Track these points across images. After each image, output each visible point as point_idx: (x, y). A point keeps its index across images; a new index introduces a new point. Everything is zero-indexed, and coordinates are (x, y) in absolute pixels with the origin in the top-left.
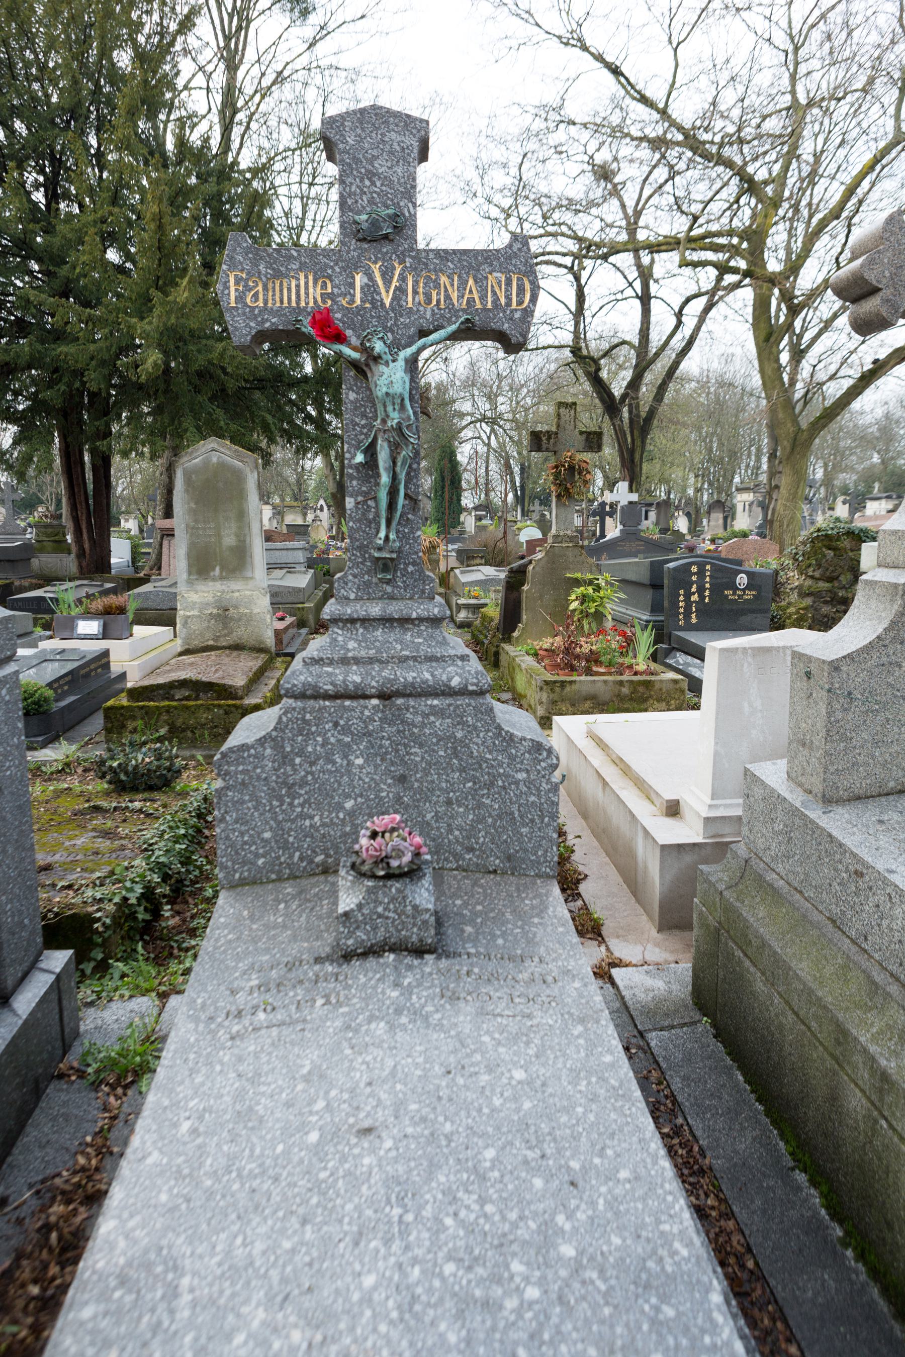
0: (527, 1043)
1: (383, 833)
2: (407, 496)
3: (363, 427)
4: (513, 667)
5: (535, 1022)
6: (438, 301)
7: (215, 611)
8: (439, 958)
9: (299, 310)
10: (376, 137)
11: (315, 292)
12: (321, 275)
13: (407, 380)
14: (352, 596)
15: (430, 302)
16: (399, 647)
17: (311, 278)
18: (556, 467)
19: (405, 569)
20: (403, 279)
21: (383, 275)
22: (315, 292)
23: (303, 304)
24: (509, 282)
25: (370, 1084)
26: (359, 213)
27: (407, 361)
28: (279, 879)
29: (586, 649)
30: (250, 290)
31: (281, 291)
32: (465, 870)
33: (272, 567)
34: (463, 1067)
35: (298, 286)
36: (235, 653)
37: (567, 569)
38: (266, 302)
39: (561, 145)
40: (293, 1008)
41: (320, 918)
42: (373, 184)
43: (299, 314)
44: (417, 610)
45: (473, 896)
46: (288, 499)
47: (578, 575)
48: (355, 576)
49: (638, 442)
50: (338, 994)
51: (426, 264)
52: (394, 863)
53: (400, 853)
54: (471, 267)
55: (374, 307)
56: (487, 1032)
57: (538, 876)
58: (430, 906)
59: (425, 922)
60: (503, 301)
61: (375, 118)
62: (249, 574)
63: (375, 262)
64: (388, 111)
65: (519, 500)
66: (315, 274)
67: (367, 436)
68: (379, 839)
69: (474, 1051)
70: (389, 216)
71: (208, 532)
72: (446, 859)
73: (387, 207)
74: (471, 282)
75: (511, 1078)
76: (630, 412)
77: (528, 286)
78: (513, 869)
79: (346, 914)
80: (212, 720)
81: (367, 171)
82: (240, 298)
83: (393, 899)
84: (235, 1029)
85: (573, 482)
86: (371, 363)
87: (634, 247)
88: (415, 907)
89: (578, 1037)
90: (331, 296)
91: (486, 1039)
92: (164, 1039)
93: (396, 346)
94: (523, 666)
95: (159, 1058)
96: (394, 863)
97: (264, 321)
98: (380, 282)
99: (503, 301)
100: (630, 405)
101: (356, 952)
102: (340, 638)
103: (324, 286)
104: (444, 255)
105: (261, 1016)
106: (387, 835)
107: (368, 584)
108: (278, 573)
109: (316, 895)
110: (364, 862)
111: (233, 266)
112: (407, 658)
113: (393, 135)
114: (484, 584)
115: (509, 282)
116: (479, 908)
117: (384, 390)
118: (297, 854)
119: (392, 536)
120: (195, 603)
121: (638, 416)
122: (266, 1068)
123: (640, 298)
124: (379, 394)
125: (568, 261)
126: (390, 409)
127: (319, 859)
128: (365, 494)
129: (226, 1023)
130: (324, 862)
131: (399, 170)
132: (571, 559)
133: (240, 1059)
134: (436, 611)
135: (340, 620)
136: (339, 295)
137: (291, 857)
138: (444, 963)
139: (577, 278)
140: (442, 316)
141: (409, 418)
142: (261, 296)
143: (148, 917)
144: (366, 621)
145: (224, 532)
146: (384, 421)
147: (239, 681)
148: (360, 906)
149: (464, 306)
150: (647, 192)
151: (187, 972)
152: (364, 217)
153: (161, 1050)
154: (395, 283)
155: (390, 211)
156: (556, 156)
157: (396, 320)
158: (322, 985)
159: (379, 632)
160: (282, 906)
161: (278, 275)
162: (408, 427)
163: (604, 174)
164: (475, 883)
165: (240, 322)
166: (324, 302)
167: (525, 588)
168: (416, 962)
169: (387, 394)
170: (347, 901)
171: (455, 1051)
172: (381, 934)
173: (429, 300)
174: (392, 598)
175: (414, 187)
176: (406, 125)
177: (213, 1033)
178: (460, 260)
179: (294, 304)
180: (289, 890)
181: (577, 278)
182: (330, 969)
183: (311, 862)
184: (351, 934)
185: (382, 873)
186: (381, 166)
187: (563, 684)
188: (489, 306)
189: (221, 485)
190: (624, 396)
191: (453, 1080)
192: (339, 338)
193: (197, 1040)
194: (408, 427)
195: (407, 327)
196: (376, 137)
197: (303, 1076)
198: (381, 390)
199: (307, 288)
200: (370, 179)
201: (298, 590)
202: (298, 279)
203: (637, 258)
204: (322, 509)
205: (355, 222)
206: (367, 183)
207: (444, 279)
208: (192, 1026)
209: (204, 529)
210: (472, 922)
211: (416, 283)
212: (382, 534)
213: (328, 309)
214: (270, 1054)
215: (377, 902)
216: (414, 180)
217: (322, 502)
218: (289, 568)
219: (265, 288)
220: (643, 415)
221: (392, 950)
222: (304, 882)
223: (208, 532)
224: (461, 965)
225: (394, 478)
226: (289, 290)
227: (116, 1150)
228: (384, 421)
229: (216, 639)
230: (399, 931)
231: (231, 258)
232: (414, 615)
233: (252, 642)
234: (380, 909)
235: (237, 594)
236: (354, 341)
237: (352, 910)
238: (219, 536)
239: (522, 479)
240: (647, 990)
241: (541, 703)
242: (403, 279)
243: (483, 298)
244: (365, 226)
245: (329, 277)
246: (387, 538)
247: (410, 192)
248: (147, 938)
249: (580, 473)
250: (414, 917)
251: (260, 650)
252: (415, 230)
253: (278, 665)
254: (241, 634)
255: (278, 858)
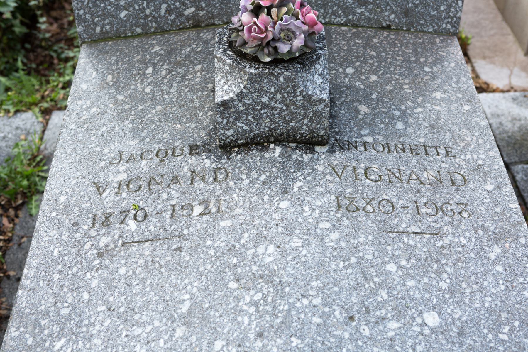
0: (439, 273)
1: (269, 8)
5: (446, 241)
8: (331, 151)
25: (260, 335)
28: (146, 34)
32: (355, 26)
34: (368, 311)
40: (167, 215)
41: (193, 89)
45: (365, 61)
50: (218, 201)
52: (284, 48)
53: (289, 35)
56: (394, 259)
57: (437, 33)
58: (325, 96)
59: (318, 114)
68: (263, 16)
69: (379, 287)
72: (334, 13)
75: (424, 324)
78: (410, 25)
79: (224, 104)
83: (280, 89)
84: (104, 241)
88: (307, 98)
89: (495, 262)
91: (391, 267)
92: (48, 159)
95: (45, 178)
96: (284, 48)
101: (237, 140)
105: (132, 225)
106: (274, 10)
109: (188, 56)
110: (245, 43)
116: (374, 78)
118: (164, 6)
122: (139, 301)
127: (189, 12)
129: (93, 233)
130: (195, 16)
133: (110, 286)
137: (157, 9)
138: (338, 158)
143: (24, 30)
148: (241, 96)
151: (67, 85)
153: (47, 171)
158: (199, 184)
160: (150, 70)
164: (367, 44)
168: (306, 158)
170: (226, 89)
171: (357, 287)
172: (265, 125)
177: (79, 245)
180: (157, 48)
182: (208, 162)
183: (181, 15)
184: (230, 125)
185: (268, 59)
191: (357, 329)
193: (62, 255)
197: (182, 317)
208: (54, 233)
210: (366, 98)
214: (143, 280)
215: (262, 92)
221: (279, 141)
222: (174, 38)
224: (358, 159)
227: (12, 273)
230: (287, 122)
234: (265, 99)
237: (232, 100)
240: (514, 120)
248: (28, 46)
250: (305, 108)
255: (143, 10)
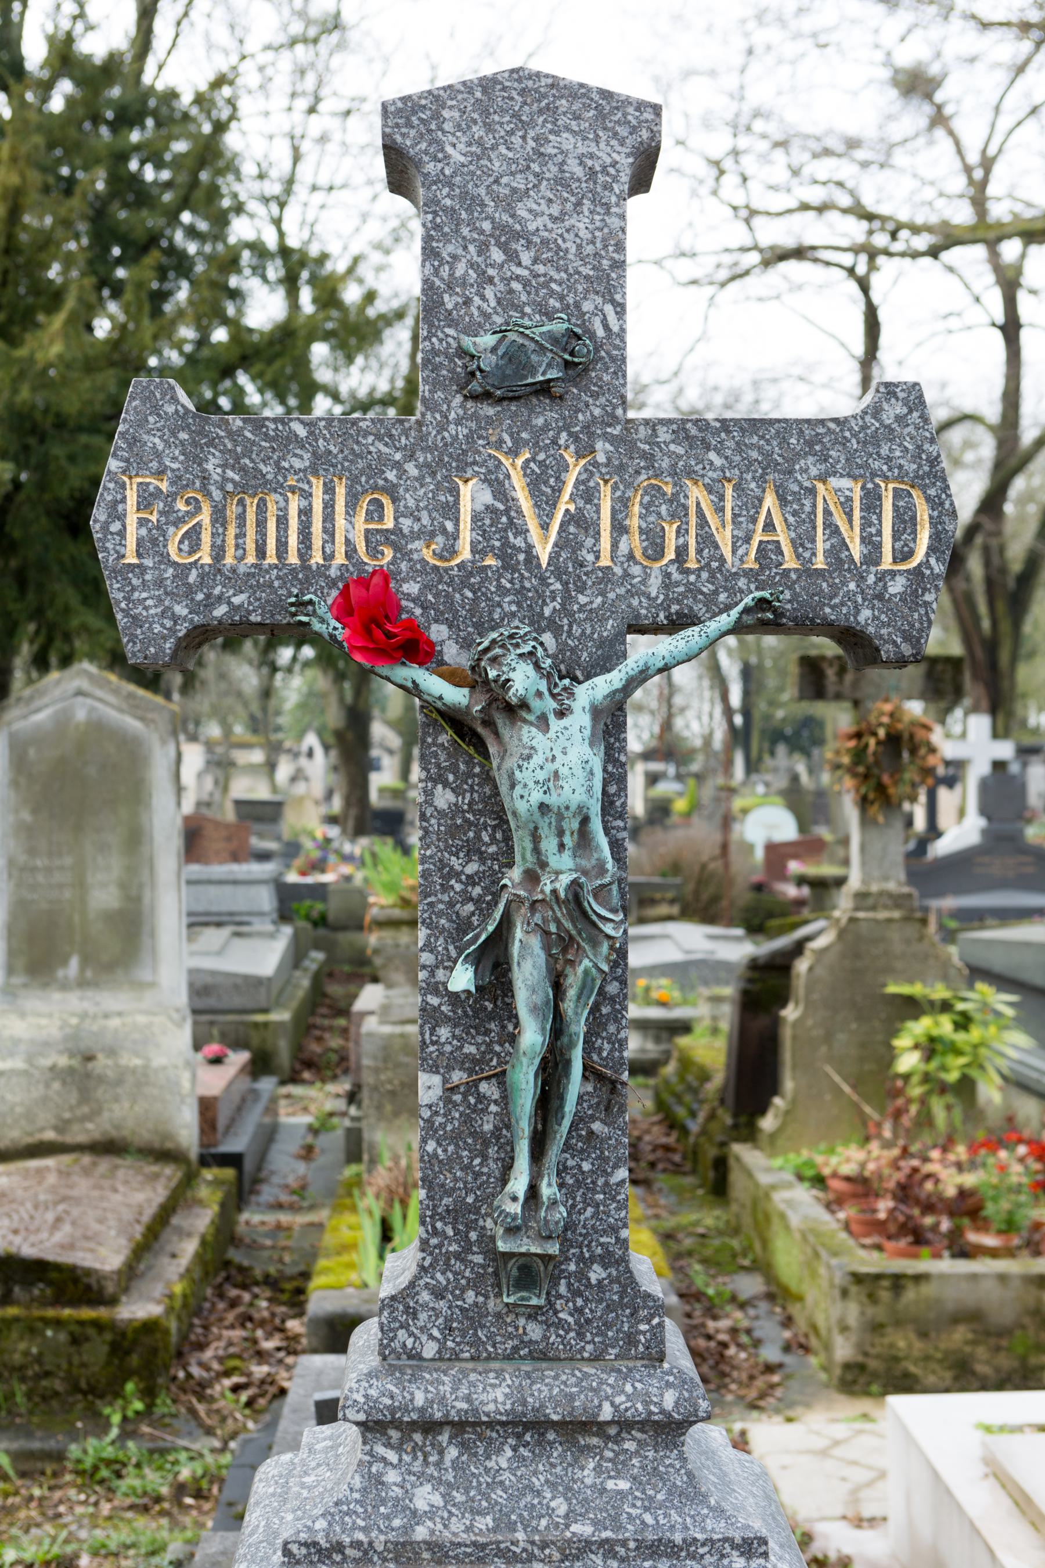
2: (588, 1069)
3: (471, 880)
4: (762, 1217)
6: (681, 552)
7: (63, 1061)
9: (306, 574)
10: (522, 145)
11: (353, 527)
12: (368, 484)
13: (597, 764)
14: (430, 1350)
15: (660, 554)
16: (560, 1506)
17: (341, 491)
18: (858, 735)
19: (582, 1275)
20: (587, 494)
21: (534, 485)
22: (353, 527)
23: (317, 558)
24: (872, 502)
26: (473, 330)
27: (596, 712)
29: (951, 1182)
30: (178, 522)
31: (261, 524)
33: (199, 921)
35: (306, 513)
36: (105, 1164)
37: (889, 971)
38: (219, 552)
39: (828, 30)
42: (513, 257)
43: (305, 584)
44: (615, 1394)
46: (238, 729)
47: (916, 989)
48: (438, 1294)
49: (1005, 627)
51: (649, 457)
54: (768, 464)
55: (508, 564)
60: (857, 550)
61: (520, 101)
62: (144, 974)
63: (514, 452)
64: (555, 83)
65: (739, 737)
66: (354, 480)
67: (484, 910)
70: (554, 339)
71: (58, 877)
73: (549, 315)
74: (770, 501)
76: (987, 563)
77: (923, 512)
80: (39, 1359)
81: (500, 228)
82: (152, 543)
85: (897, 769)
86: (500, 720)
87: (986, 233)
90: (395, 538)
93: (566, 672)
94: (795, 1220)
97: (211, 602)
98: (525, 503)
99: (857, 550)
100: (986, 551)
102: (392, 1476)
103: (376, 511)
104: (695, 432)
107: (474, 1317)
108: (213, 937)
111: (136, 463)
112: (586, 1546)
113: (567, 141)
114: (680, 972)
115: (872, 502)
117: (536, 796)
119: (548, 1190)
120: (16, 1042)
121: (1003, 570)
123: (1002, 328)
124: (521, 807)
125: (847, 259)
126: (549, 845)
128: (472, 1065)
131: (581, 224)
132: (898, 948)
134: (669, 1400)
135: (396, 1424)
136: (415, 536)
139: (864, 286)
140: (693, 590)
141: (602, 870)
142: (206, 538)
144: (467, 1428)
145: (94, 878)
146: (532, 878)
147: (107, 1258)
149: (751, 564)
150: (1005, 123)
152: (488, 340)
154: (565, 505)
155: (558, 327)
156: (816, 51)
157: (567, 598)
159: (503, 1459)
161: (253, 483)
162: (597, 893)
163: (917, 84)
165: (148, 604)
166: (374, 552)
167: (790, 1013)
169: (543, 808)
173: (656, 551)
174: (542, 1355)
175: (620, 265)
176: (601, 116)
178: (739, 447)
179: (293, 559)
181: (864, 286)
186: (535, 214)
187: (898, 1282)
188: (820, 563)
189: (92, 771)
190: (972, 530)
192: (417, 649)
194: (597, 893)
195: (595, 616)
196: (522, 145)
198: (523, 800)
199: (329, 517)
200: (504, 247)
201: (255, 983)
202: (308, 495)
203: (994, 256)
204: (310, 754)
205: (462, 352)
206: (497, 255)
207: (696, 494)
209: (49, 870)
211: (622, 505)
212: (519, 1184)
213: (386, 577)
216: (620, 247)
217: (311, 740)
218: (235, 922)
219: (219, 517)
220: (1016, 567)
223: (58, 877)
225: (558, 1029)
226: (282, 521)
228: (532, 878)
229: (62, 1127)
231: (133, 442)
232: (607, 1413)
233: (145, 1135)
235: (115, 1022)
236: (452, 653)
238: (81, 885)
239: (747, 694)
241: (844, 1329)
242: (587, 494)
243: (802, 542)
244: (488, 362)
245: (391, 491)
246: (533, 1191)
247: (608, 278)
249: (913, 751)
251: (164, 1154)
252: (620, 371)
253: (203, 1192)
254: (120, 1115)
